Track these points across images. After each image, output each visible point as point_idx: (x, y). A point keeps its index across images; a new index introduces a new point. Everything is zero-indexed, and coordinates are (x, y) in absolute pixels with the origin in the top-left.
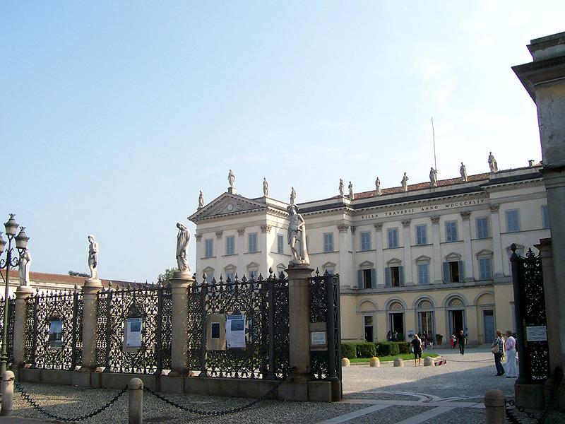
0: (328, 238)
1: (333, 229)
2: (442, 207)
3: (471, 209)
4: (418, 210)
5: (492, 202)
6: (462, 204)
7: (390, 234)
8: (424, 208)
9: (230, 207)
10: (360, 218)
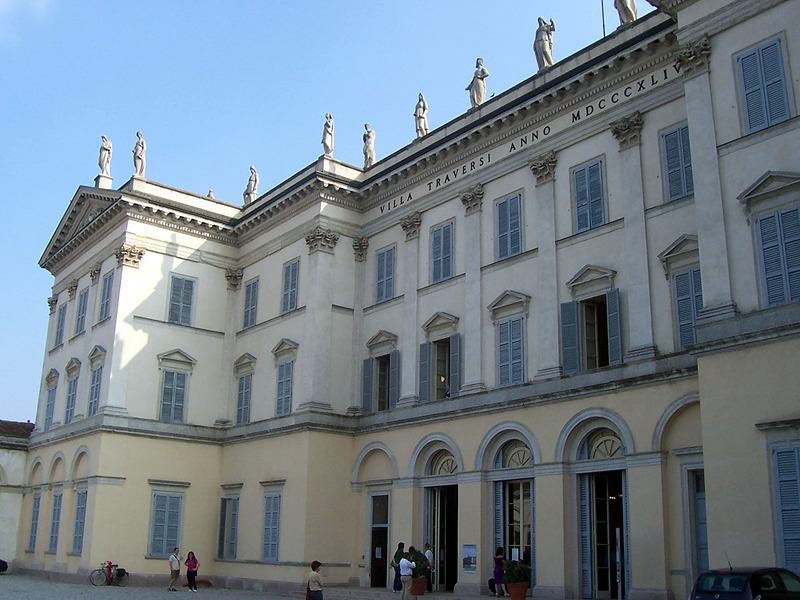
0: (292, 272)
1: (300, 248)
3: (640, 106)
7: (436, 240)
8: (517, 142)
10: (376, 213)
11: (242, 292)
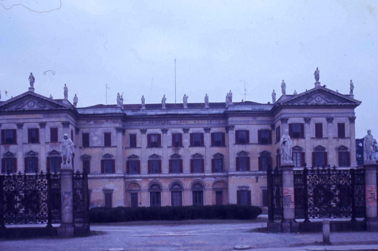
2: (192, 122)
5: (230, 123)
6: (205, 123)
11: (81, 136)
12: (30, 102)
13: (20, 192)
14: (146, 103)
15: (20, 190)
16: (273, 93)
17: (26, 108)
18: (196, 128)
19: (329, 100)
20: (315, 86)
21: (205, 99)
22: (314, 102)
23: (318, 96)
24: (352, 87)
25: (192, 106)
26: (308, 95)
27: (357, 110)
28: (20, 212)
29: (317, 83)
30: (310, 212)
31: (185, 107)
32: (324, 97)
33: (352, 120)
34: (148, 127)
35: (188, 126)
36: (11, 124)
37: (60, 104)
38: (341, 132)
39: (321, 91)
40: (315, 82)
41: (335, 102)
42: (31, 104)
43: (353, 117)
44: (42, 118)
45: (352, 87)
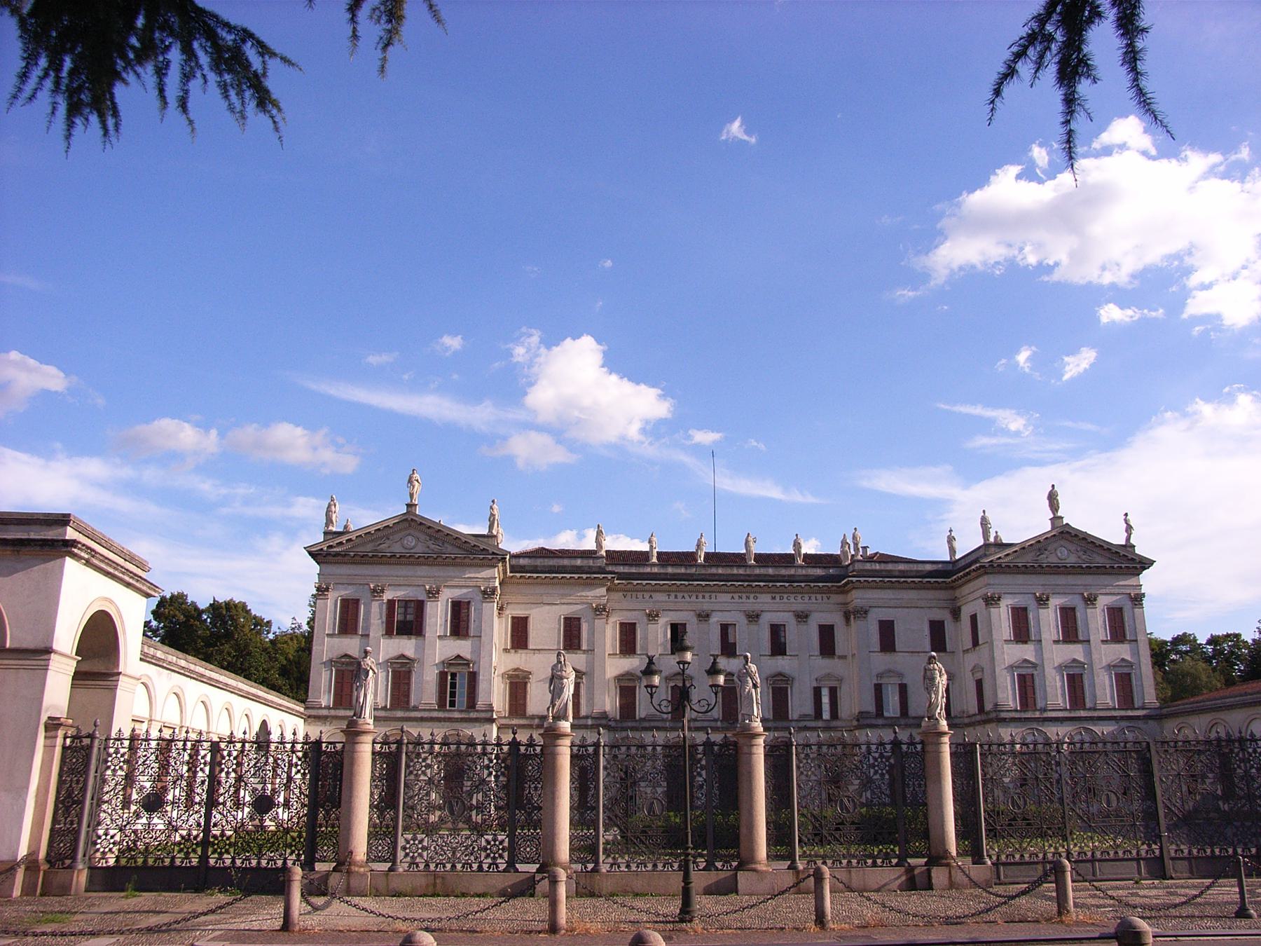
2: (765, 598)
4: (726, 597)
6: (799, 603)
9: (410, 541)
12: (410, 538)
13: (642, 784)
14: (803, 551)
15: (873, 793)
16: (948, 537)
17: (397, 548)
18: (776, 609)
19: (1084, 557)
20: (1053, 524)
21: (794, 545)
22: (1053, 559)
23: (1062, 546)
24: (1129, 529)
25: (763, 559)
26: (1039, 545)
27: (1147, 580)
28: (480, 822)
29: (1056, 519)
30: (702, 769)
31: (800, 562)
32: (1073, 547)
33: (1137, 599)
34: (763, 608)
35: (757, 607)
36: (891, 609)
37: (1130, 556)
38: (1119, 627)
39: (1064, 534)
40: (1052, 516)
41: (1099, 560)
42: (410, 541)
43: (1137, 594)
44: (424, 576)
45: (1129, 529)
